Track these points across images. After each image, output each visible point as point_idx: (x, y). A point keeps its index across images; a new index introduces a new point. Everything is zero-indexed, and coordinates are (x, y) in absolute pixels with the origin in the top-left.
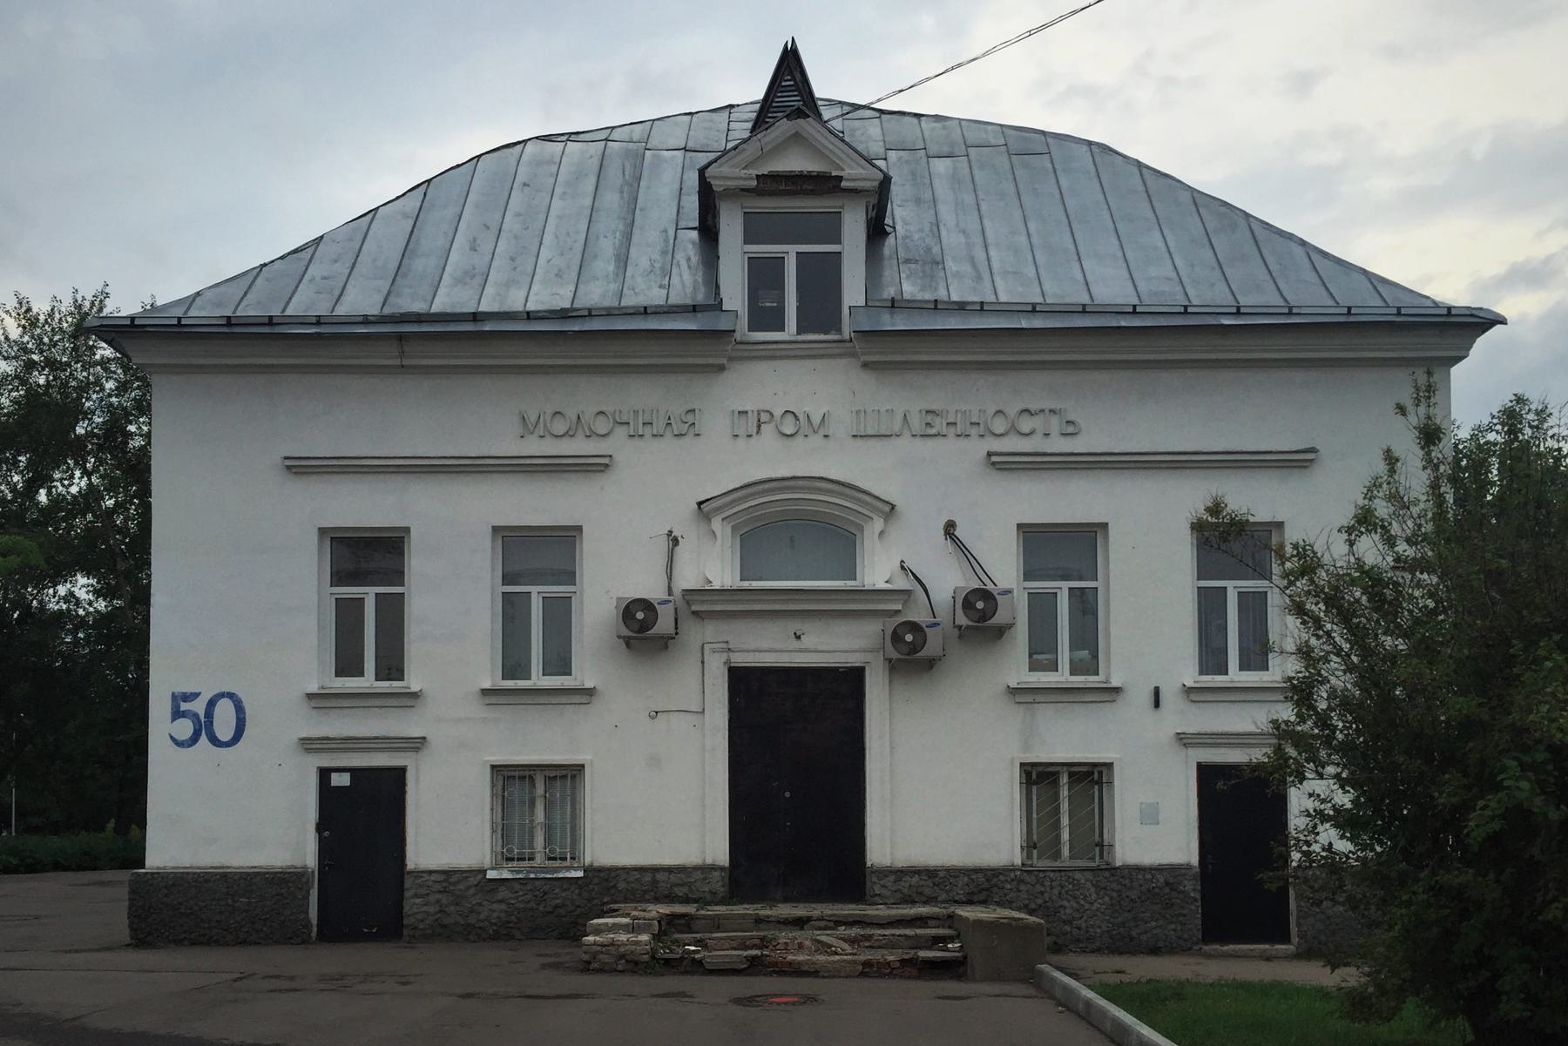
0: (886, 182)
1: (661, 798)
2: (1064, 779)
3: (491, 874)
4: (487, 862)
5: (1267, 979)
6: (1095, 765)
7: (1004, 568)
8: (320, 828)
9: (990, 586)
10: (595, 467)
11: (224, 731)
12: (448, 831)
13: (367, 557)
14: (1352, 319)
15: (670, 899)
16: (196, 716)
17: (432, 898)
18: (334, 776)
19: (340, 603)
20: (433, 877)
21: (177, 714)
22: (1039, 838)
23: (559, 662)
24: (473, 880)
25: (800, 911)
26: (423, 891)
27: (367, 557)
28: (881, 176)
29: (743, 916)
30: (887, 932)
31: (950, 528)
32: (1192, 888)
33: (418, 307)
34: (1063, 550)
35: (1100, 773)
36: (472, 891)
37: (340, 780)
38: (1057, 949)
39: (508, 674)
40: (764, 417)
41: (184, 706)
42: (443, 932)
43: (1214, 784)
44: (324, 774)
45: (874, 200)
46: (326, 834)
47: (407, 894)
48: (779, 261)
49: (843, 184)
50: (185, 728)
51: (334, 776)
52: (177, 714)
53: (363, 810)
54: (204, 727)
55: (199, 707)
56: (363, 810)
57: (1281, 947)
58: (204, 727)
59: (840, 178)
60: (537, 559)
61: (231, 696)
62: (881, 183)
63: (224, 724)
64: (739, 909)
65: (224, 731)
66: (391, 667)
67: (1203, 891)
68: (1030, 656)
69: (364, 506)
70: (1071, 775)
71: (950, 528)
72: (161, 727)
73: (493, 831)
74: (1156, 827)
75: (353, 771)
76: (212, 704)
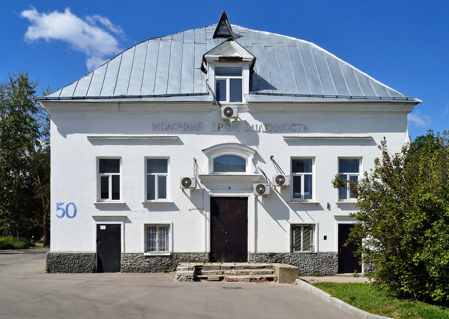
0: (255, 60)
1: (192, 233)
2: (302, 229)
3: (145, 254)
4: (143, 251)
5: (348, 282)
6: (311, 224)
7: (287, 171)
8: (97, 241)
9: (283, 175)
10: (178, 142)
11: (71, 213)
12: (133, 243)
13: (109, 165)
14: (408, 101)
15: (194, 261)
16: (63, 209)
17: (128, 261)
18: (101, 226)
19: (102, 178)
20: (129, 255)
21: (58, 209)
22: (295, 246)
23: (163, 195)
24: (140, 256)
25: (232, 264)
26: (126, 259)
27: (109, 165)
28: (253, 57)
29: (217, 266)
30: (256, 270)
31: (272, 157)
32: (335, 257)
33: (124, 93)
34: (300, 165)
35: (312, 227)
36: (139, 259)
37: (103, 228)
38: (300, 275)
39: (148, 198)
40: (221, 126)
41: (60, 207)
42: (130, 270)
43: (344, 230)
44: (98, 226)
45: (251, 64)
46: (99, 242)
47: (122, 259)
48: (225, 81)
49: (243, 60)
50: (60, 213)
51: (101, 226)
52: (58, 209)
53: (109, 237)
54: (65, 213)
55: (64, 207)
56: (109, 237)
57: (122, 227)
58: (65, 213)
59: (242, 58)
60: (156, 165)
61: (73, 204)
62: (253, 59)
63: (71, 212)
64: (214, 264)
65: (71, 213)
66: (116, 196)
67: (338, 259)
68: (294, 194)
69: (109, 151)
70: (304, 227)
71: (272, 157)
72: (54, 213)
73: (145, 242)
74: (327, 243)
75: (106, 225)
76: (67, 206)
